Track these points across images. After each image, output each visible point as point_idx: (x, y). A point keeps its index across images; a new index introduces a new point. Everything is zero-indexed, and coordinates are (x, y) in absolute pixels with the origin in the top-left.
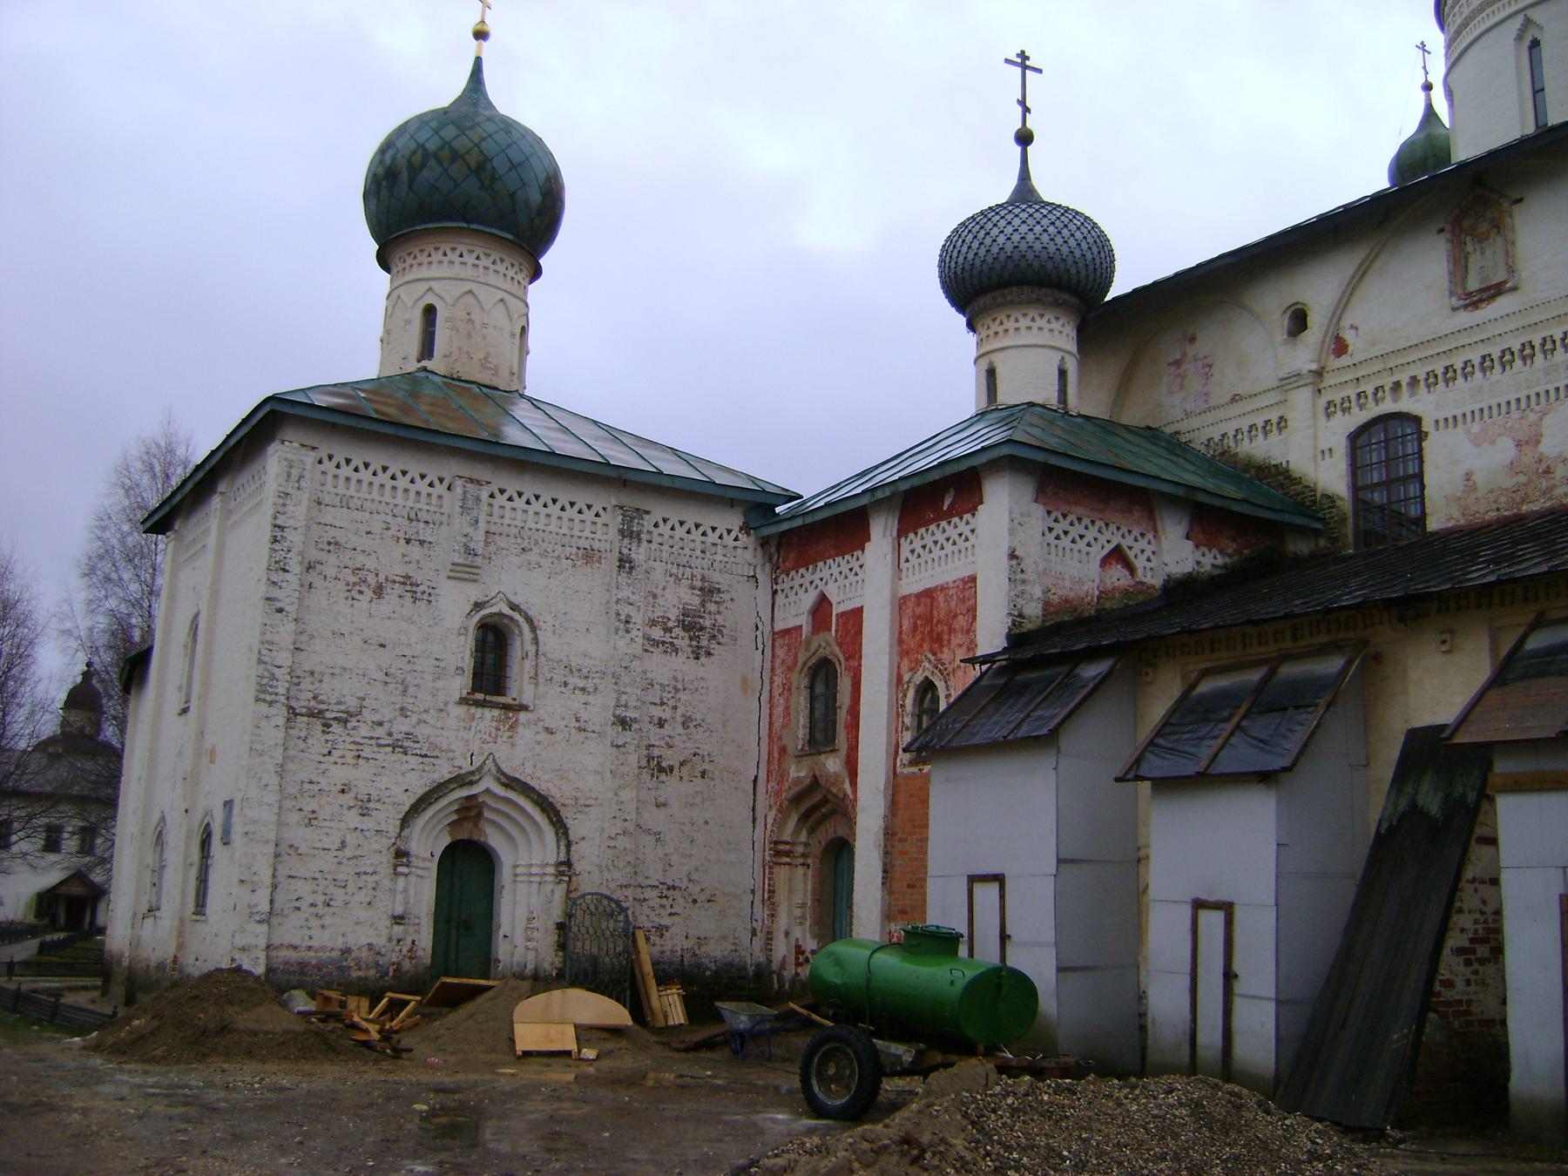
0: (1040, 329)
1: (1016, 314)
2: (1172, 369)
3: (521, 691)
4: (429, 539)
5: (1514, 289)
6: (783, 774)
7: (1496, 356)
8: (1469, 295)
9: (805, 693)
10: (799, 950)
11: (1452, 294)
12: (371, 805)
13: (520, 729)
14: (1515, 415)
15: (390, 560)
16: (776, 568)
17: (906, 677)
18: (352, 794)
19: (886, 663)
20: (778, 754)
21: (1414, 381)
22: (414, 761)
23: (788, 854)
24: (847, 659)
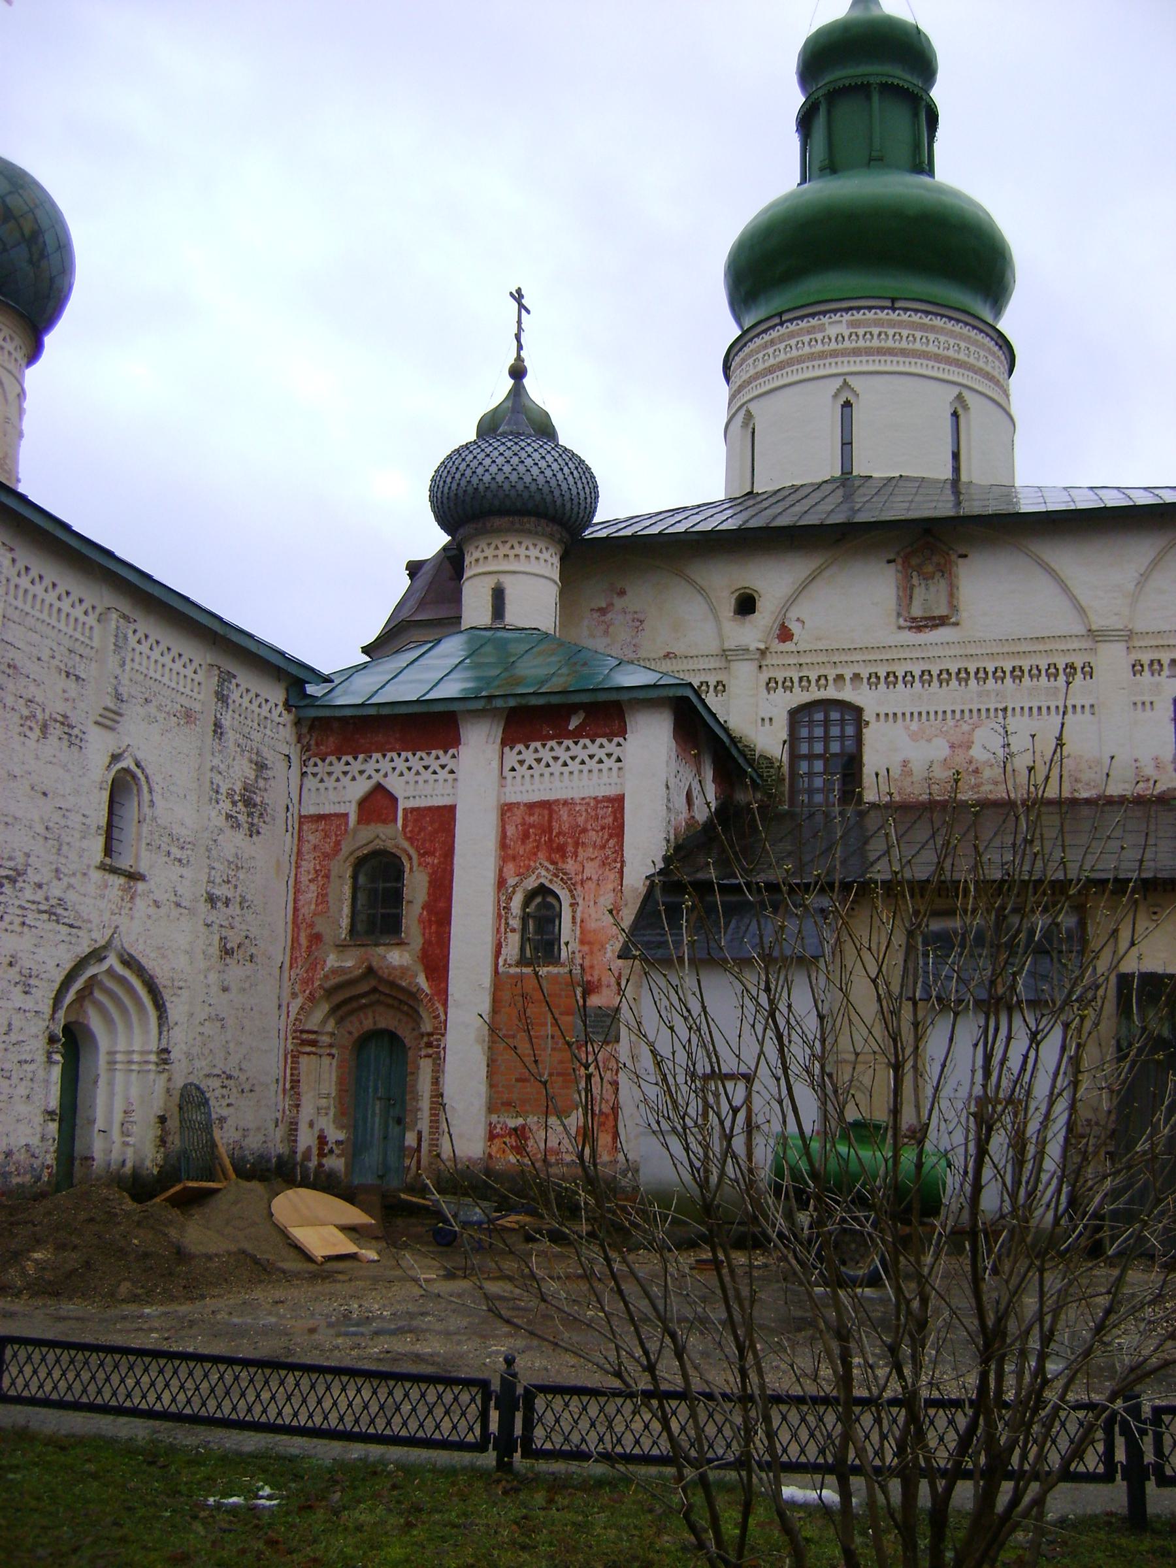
0: (506, 556)
1: (527, 542)
2: (596, 615)
3: (137, 857)
4: (83, 676)
5: (956, 624)
6: (313, 965)
7: (935, 673)
8: (914, 619)
9: (349, 882)
10: (322, 1139)
11: (899, 615)
12: (32, 982)
13: (138, 900)
14: (950, 723)
15: (53, 695)
16: (306, 749)
17: (512, 881)
18: (17, 969)
19: (492, 867)
20: (307, 941)
21: (856, 677)
22: (64, 930)
23: (314, 1043)
24: (421, 855)
